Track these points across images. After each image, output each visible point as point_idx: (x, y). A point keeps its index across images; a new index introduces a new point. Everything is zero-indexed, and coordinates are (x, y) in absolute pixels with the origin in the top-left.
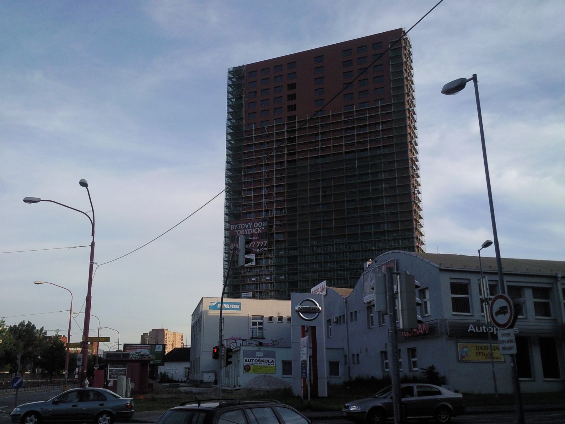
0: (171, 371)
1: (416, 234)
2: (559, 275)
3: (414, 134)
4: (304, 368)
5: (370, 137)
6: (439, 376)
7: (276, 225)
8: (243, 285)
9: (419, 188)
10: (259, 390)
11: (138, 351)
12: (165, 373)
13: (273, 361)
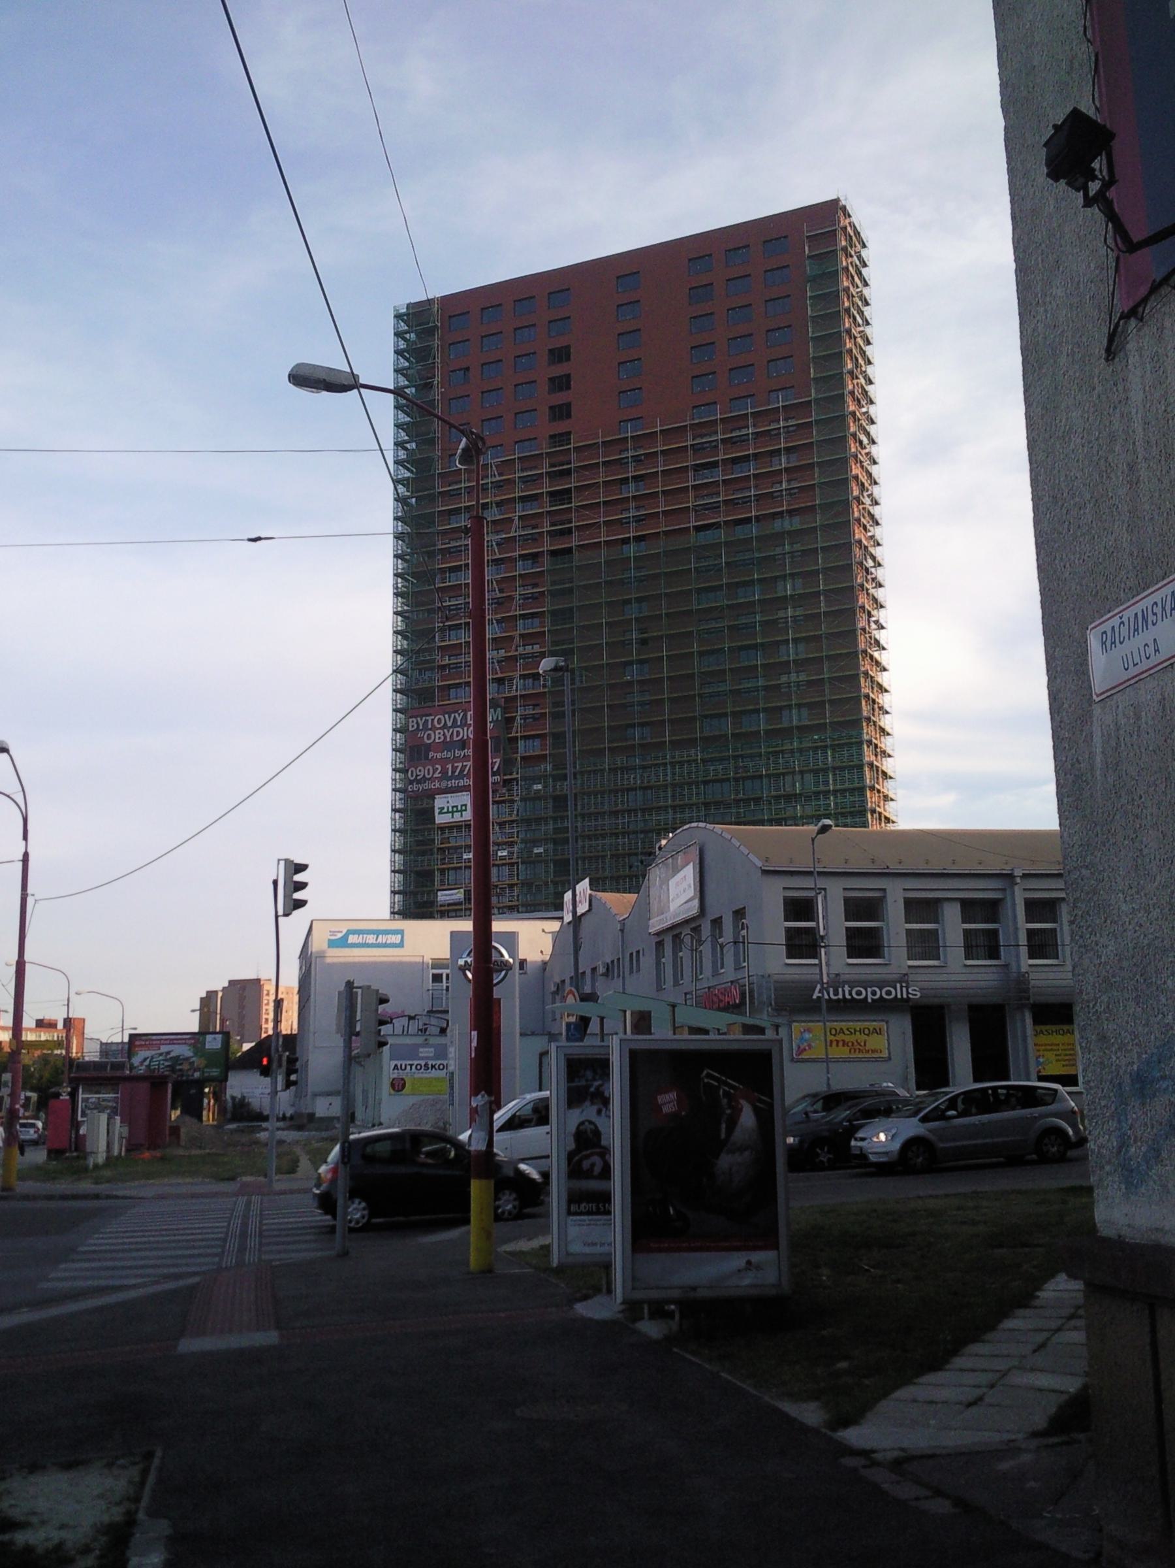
1: (867, 732)
2: (1018, 872)
7: (524, 717)
8: (442, 871)
11: (164, 1049)
12: (243, 1098)
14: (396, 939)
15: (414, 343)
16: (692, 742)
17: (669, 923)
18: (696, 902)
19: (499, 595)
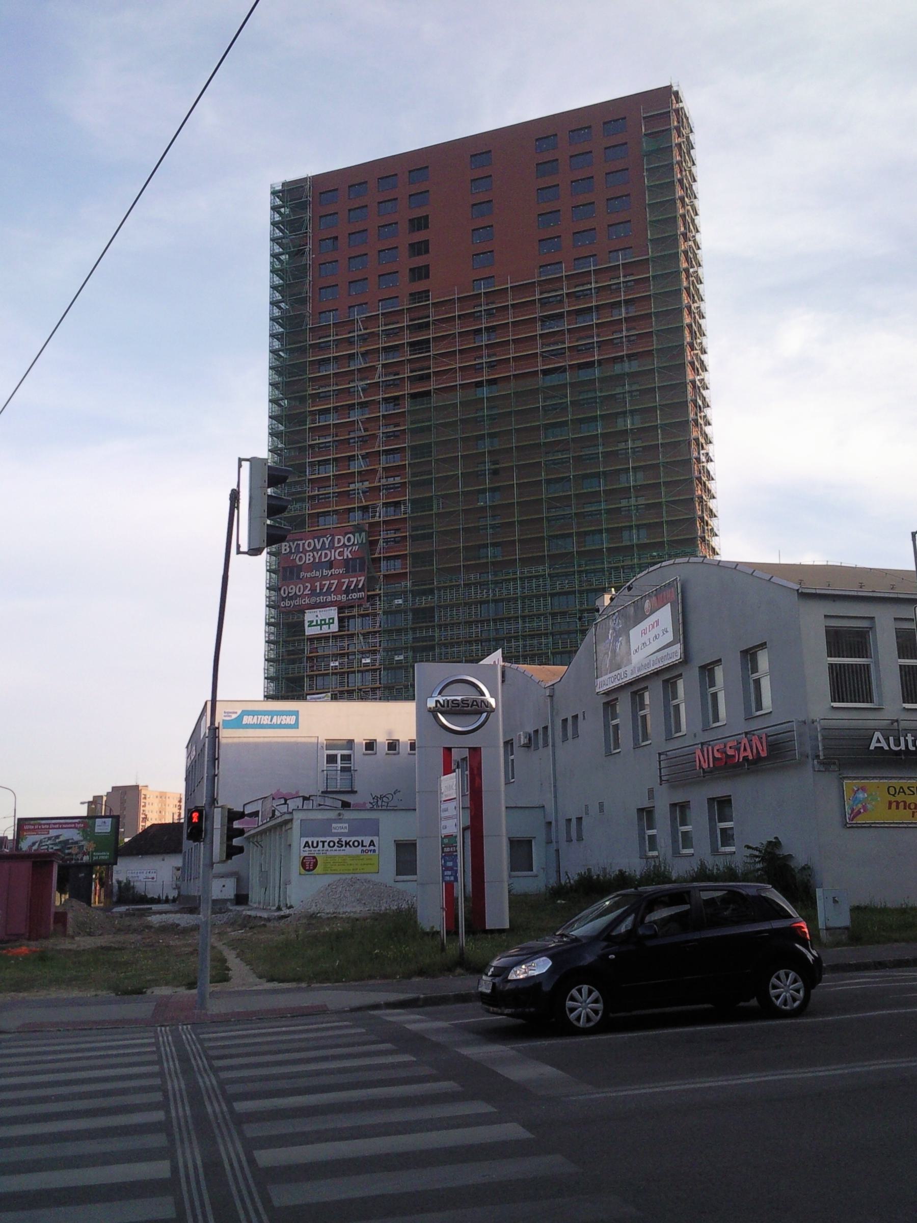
0: (142, 877)
3: (700, 326)
4: (449, 856)
5: (598, 336)
6: (793, 864)
7: (386, 541)
8: (311, 677)
9: (710, 449)
10: (334, 918)
11: (53, 833)
12: (129, 882)
13: (372, 843)
14: (291, 720)
15: (288, 216)
16: (540, 560)
17: (630, 677)
18: (678, 648)
19: (364, 434)
